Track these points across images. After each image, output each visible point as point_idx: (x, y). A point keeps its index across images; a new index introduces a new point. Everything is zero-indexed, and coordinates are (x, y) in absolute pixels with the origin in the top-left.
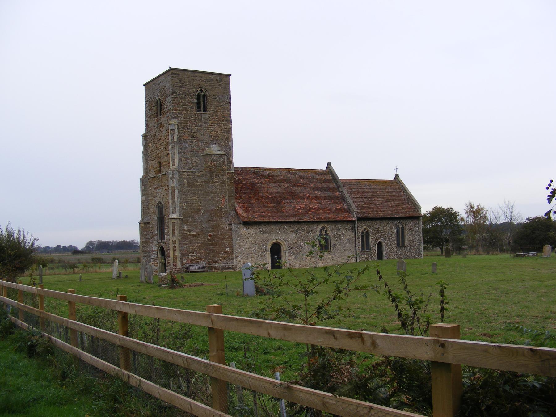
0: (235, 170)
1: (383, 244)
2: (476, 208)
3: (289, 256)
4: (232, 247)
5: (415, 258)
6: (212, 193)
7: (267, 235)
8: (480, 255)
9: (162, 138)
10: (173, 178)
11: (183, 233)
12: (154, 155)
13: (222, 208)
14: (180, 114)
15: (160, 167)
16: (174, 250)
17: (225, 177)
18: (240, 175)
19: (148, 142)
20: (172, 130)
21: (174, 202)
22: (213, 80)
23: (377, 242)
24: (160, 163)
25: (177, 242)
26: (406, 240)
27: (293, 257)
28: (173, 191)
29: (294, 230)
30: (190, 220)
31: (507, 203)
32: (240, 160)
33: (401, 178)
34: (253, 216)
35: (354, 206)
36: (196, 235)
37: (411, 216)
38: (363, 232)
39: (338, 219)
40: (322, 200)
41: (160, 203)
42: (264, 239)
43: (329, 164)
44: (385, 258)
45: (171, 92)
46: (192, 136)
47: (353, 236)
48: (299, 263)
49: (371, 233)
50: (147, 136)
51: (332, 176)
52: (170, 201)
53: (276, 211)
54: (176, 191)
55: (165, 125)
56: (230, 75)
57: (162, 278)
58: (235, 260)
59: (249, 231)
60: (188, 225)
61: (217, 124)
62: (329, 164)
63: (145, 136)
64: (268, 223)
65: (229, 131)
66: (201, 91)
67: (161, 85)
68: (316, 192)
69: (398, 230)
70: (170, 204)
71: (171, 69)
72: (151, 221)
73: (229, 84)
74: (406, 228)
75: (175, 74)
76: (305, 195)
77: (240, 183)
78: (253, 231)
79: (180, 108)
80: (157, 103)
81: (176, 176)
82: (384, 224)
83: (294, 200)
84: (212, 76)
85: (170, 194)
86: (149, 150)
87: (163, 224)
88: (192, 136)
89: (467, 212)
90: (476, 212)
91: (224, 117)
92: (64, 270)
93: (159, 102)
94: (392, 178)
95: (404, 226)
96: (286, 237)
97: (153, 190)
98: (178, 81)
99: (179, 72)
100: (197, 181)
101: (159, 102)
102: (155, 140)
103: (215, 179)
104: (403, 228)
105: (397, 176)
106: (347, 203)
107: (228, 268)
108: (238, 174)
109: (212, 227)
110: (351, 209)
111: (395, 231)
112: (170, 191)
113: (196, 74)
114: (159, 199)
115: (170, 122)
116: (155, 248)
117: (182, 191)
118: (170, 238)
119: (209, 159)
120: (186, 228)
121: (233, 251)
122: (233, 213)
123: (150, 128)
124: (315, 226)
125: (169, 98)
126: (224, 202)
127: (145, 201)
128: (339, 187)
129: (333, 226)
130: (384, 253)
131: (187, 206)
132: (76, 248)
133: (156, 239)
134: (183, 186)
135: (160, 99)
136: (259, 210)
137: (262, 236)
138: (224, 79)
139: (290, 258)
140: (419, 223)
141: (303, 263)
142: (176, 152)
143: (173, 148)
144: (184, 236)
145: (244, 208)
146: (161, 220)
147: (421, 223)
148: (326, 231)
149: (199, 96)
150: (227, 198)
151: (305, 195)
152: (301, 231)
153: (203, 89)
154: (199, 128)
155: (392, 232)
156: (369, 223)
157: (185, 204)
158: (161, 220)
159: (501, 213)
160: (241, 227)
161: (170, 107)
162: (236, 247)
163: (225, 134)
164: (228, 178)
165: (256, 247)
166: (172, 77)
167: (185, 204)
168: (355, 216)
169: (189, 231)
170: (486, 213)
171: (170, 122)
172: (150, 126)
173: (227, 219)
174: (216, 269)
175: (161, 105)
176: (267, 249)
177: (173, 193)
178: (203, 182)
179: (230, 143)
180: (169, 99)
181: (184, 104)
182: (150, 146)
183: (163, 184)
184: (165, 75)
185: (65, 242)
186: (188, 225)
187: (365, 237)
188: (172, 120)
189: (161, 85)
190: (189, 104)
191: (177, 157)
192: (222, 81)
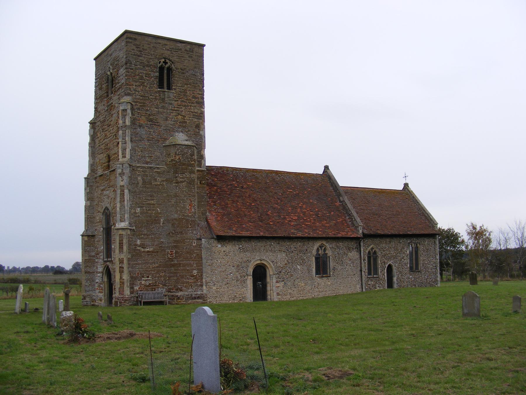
0: (207, 170)
2: (478, 229)
3: (277, 282)
4: (202, 269)
5: (431, 286)
6: (176, 196)
7: (248, 254)
8: (487, 281)
9: (112, 123)
10: (122, 174)
11: (135, 250)
12: (102, 147)
13: (188, 216)
14: (135, 90)
15: (109, 161)
16: (121, 272)
17: (194, 176)
18: (215, 175)
19: (96, 130)
20: (123, 110)
21: (122, 206)
22: (181, 49)
23: (387, 266)
24: (109, 157)
25: (125, 261)
26: (421, 262)
27: (281, 284)
28: (122, 191)
29: (284, 248)
30: (145, 232)
31: (518, 223)
32: (215, 156)
33: (412, 187)
34: (230, 229)
35: (358, 220)
36: (153, 252)
37: (426, 233)
38: (369, 252)
39: (340, 235)
40: (319, 211)
41: (107, 208)
42: (245, 259)
43: (326, 168)
44: (395, 286)
45: (124, 62)
46: (151, 120)
47: (358, 257)
48: (290, 291)
49: (379, 253)
50: (95, 123)
51: (330, 182)
52: (118, 205)
53: (260, 223)
54: (126, 191)
55: (116, 105)
56: (204, 46)
57: (64, 320)
58: (204, 287)
59: (224, 248)
60: (142, 238)
61: (185, 106)
62: (326, 168)
63: (92, 123)
65: (201, 116)
66: (165, 63)
67: (113, 56)
68: (311, 201)
70: (118, 209)
71: (126, 32)
72: (96, 233)
73: (202, 56)
74: (421, 248)
75: (131, 38)
76: (298, 204)
77: (215, 186)
78: (230, 248)
79: (136, 82)
80: (108, 79)
81: (127, 171)
82: (394, 243)
83: (283, 209)
84: (179, 45)
85: (118, 196)
86: (97, 141)
87: (111, 237)
88: (151, 120)
89: (469, 233)
90: (478, 234)
91: (194, 97)
92: (5, 293)
93: (110, 78)
94: (400, 187)
96: (273, 257)
97: (100, 192)
98: (134, 47)
99: (137, 37)
100: (156, 180)
101: (110, 78)
102: (104, 127)
103: (180, 177)
104: (417, 248)
105: (406, 185)
106: (350, 215)
107: (195, 298)
108: (212, 175)
109: (175, 241)
110: (355, 222)
112: (119, 192)
113: (160, 41)
114: (106, 203)
115: (122, 101)
116: (100, 269)
117: (135, 192)
118: (116, 255)
119: (172, 151)
120: (139, 242)
121: (202, 275)
122: (203, 224)
123: (99, 112)
124: (311, 243)
125: (122, 70)
126: (191, 208)
127: (89, 206)
128: (339, 195)
129: (334, 244)
130: (395, 279)
131: (141, 213)
132: (64, 268)
133: (102, 257)
134: (137, 186)
135: (111, 74)
136: (238, 221)
137: (242, 255)
138: (196, 49)
139: (278, 285)
140: (435, 242)
141: (295, 292)
142: (128, 139)
143: (124, 134)
144: (135, 254)
145: (219, 218)
146: (108, 231)
147: (437, 242)
148: (325, 250)
149: (161, 69)
150: (196, 203)
151: (298, 204)
152: (292, 250)
153: (167, 61)
154: (161, 110)
155: (404, 253)
156: (377, 241)
157: (138, 210)
158: (108, 231)
159: (511, 235)
160: (214, 243)
161: (123, 81)
162: (206, 269)
163: (196, 120)
164: (198, 178)
165: (234, 269)
166: (127, 42)
167: (138, 210)
168: (361, 231)
169: (143, 246)
170: (490, 235)
171: (122, 101)
172: (99, 110)
173: (194, 232)
174: (179, 298)
175: (112, 81)
176: (248, 273)
177: (122, 195)
178: (163, 181)
179: (201, 132)
180: (122, 71)
181: (142, 78)
182: (99, 135)
183: (111, 184)
184: (119, 41)
185: (54, 263)
186: (142, 238)
187: (372, 258)
188: (125, 97)
189: (113, 56)
191: (129, 146)
192: (194, 52)
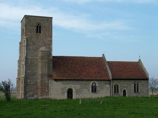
1: (126, 91)
3: (76, 94)
39: (102, 79)
42: (64, 87)
43: (103, 55)
49: (119, 85)
54: (24, 66)
56: (52, 18)
59: (57, 83)
61: (45, 38)
62: (103, 55)
64: (66, 80)
65: (51, 41)
66: (39, 24)
69: (135, 85)
74: (140, 84)
75: (27, 18)
78: (59, 83)
82: (127, 82)
95: (139, 83)
98: (28, 20)
104: (138, 84)
105: (140, 60)
111: (133, 85)
120: (29, 81)
124: (90, 82)
129: (99, 82)
138: (49, 19)
149: (37, 27)
155: (131, 86)
156: (119, 81)
163: (49, 42)
165: (60, 90)
190: (37, 29)
